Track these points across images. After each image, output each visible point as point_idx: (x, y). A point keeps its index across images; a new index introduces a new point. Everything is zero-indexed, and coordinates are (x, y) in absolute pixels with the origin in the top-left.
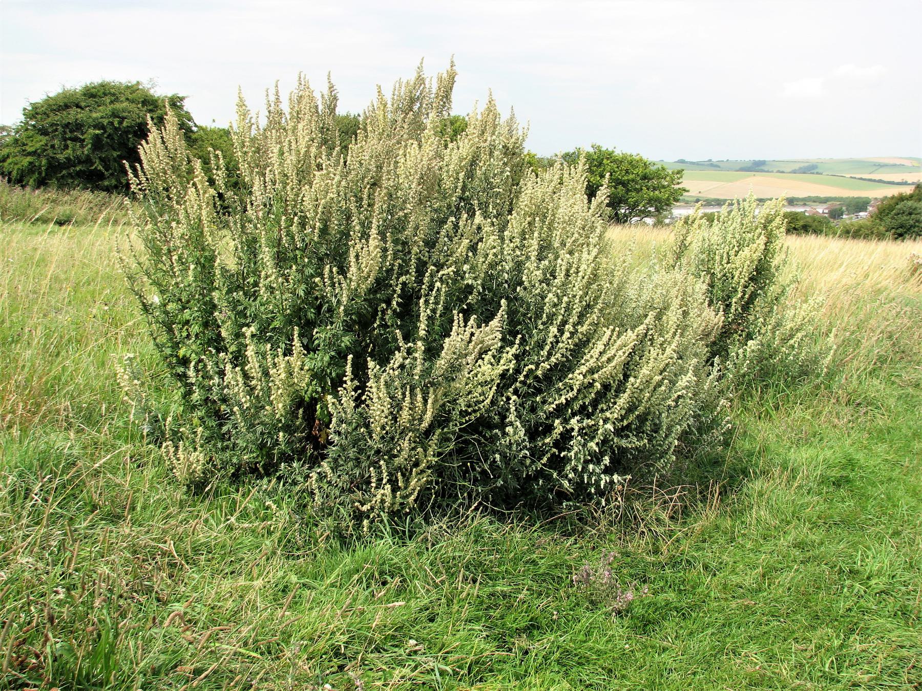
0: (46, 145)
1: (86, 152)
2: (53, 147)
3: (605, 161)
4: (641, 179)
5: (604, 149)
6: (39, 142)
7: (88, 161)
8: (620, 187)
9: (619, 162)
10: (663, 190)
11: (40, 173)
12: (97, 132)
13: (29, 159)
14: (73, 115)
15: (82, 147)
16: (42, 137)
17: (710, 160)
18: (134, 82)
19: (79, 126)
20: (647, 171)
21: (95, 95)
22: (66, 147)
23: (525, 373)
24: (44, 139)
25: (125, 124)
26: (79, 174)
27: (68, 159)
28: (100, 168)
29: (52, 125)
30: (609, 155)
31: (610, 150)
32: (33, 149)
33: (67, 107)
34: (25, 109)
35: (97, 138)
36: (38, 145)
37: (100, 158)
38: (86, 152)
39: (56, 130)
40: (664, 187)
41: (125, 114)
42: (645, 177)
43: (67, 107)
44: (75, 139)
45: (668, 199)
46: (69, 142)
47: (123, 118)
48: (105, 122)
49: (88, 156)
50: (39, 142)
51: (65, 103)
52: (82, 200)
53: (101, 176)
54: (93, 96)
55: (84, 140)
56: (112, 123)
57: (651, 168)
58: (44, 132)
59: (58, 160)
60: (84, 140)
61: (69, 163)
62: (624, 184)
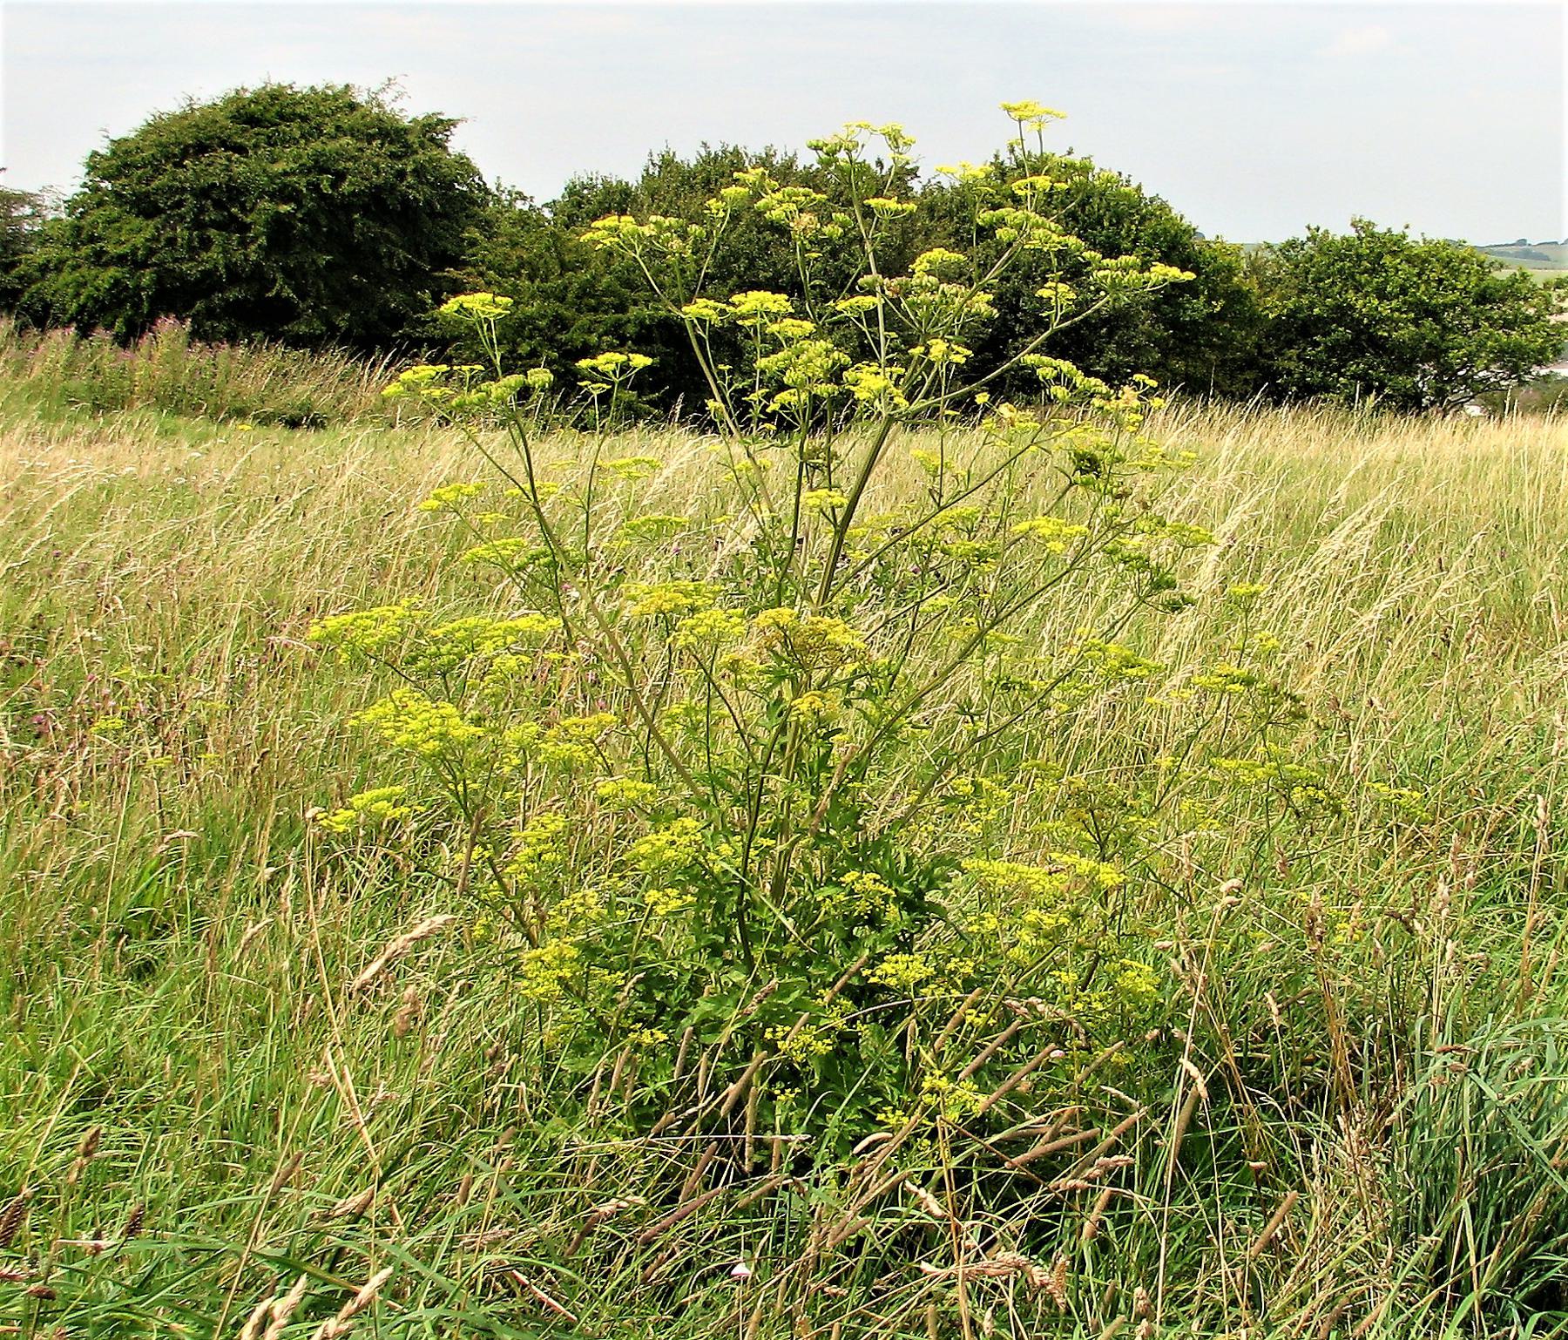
0: (155, 239)
1: (253, 257)
2: (171, 242)
3: (1387, 260)
4: (1476, 302)
5: (1380, 229)
6: (137, 233)
7: (258, 278)
8: (1428, 322)
9: (1420, 262)
10: (1527, 328)
11: (137, 306)
12: (284, 208)
13: (113, 271)
14: (216, 168)
15: (243, 243)
16: (138, 222)
17: (1522, 242)
18: (340, 87)
19: (234, 193)
20: (1487, 282)
21: (263, 117)
22: (206, 244)
23: (416, 933)
24: (149, 227)
25: (345, 187)
26: (232, 309)
27: (207, 274)
28: (288, 292)
29: (172, 191)
30: (1394, 245)
31: (1397, 231)
32: (121, 250)
33: (201, 148)
34: (95, 154)
35: (279, 225)
36: (139, 240)
37: (284, 270)
38: (253, 257)
39: (179, 204)
40: (1528, 320)
41: (342, 165)
42: (1483, 298)
43: (201, 148)
44: (224, 226)
45: (1542, 351)
46: (212, 232)
47: (340, 176)
48: (302, 183)
49: (257, 264)
50: (137, 233)
51: (187, 142)
52: (319, 378)
53: (286, 311)
54: (252, 120)
55: (247, 227)
56: (315, 187)
57: (1496, 274)
58: (145, 207)
59: (182, 277)
60: (247, 227)
61: (208, 283)
62: (1434, 313)
